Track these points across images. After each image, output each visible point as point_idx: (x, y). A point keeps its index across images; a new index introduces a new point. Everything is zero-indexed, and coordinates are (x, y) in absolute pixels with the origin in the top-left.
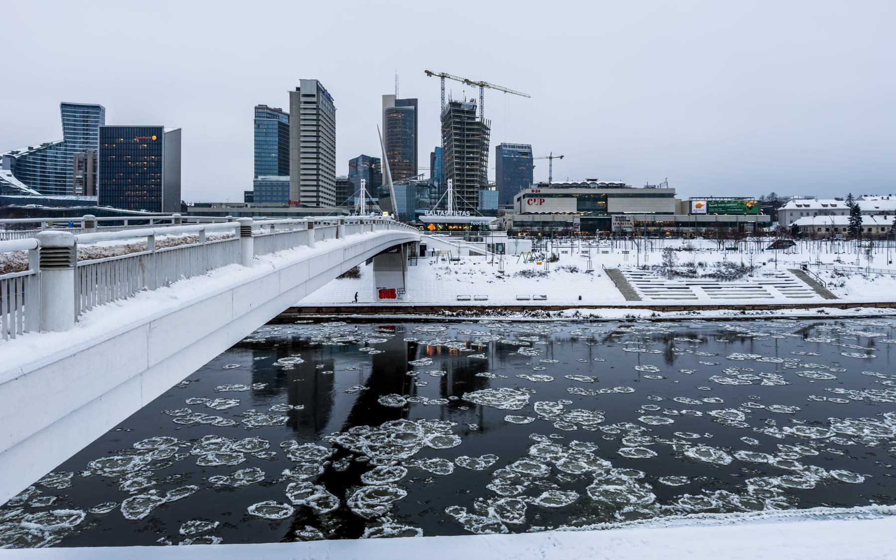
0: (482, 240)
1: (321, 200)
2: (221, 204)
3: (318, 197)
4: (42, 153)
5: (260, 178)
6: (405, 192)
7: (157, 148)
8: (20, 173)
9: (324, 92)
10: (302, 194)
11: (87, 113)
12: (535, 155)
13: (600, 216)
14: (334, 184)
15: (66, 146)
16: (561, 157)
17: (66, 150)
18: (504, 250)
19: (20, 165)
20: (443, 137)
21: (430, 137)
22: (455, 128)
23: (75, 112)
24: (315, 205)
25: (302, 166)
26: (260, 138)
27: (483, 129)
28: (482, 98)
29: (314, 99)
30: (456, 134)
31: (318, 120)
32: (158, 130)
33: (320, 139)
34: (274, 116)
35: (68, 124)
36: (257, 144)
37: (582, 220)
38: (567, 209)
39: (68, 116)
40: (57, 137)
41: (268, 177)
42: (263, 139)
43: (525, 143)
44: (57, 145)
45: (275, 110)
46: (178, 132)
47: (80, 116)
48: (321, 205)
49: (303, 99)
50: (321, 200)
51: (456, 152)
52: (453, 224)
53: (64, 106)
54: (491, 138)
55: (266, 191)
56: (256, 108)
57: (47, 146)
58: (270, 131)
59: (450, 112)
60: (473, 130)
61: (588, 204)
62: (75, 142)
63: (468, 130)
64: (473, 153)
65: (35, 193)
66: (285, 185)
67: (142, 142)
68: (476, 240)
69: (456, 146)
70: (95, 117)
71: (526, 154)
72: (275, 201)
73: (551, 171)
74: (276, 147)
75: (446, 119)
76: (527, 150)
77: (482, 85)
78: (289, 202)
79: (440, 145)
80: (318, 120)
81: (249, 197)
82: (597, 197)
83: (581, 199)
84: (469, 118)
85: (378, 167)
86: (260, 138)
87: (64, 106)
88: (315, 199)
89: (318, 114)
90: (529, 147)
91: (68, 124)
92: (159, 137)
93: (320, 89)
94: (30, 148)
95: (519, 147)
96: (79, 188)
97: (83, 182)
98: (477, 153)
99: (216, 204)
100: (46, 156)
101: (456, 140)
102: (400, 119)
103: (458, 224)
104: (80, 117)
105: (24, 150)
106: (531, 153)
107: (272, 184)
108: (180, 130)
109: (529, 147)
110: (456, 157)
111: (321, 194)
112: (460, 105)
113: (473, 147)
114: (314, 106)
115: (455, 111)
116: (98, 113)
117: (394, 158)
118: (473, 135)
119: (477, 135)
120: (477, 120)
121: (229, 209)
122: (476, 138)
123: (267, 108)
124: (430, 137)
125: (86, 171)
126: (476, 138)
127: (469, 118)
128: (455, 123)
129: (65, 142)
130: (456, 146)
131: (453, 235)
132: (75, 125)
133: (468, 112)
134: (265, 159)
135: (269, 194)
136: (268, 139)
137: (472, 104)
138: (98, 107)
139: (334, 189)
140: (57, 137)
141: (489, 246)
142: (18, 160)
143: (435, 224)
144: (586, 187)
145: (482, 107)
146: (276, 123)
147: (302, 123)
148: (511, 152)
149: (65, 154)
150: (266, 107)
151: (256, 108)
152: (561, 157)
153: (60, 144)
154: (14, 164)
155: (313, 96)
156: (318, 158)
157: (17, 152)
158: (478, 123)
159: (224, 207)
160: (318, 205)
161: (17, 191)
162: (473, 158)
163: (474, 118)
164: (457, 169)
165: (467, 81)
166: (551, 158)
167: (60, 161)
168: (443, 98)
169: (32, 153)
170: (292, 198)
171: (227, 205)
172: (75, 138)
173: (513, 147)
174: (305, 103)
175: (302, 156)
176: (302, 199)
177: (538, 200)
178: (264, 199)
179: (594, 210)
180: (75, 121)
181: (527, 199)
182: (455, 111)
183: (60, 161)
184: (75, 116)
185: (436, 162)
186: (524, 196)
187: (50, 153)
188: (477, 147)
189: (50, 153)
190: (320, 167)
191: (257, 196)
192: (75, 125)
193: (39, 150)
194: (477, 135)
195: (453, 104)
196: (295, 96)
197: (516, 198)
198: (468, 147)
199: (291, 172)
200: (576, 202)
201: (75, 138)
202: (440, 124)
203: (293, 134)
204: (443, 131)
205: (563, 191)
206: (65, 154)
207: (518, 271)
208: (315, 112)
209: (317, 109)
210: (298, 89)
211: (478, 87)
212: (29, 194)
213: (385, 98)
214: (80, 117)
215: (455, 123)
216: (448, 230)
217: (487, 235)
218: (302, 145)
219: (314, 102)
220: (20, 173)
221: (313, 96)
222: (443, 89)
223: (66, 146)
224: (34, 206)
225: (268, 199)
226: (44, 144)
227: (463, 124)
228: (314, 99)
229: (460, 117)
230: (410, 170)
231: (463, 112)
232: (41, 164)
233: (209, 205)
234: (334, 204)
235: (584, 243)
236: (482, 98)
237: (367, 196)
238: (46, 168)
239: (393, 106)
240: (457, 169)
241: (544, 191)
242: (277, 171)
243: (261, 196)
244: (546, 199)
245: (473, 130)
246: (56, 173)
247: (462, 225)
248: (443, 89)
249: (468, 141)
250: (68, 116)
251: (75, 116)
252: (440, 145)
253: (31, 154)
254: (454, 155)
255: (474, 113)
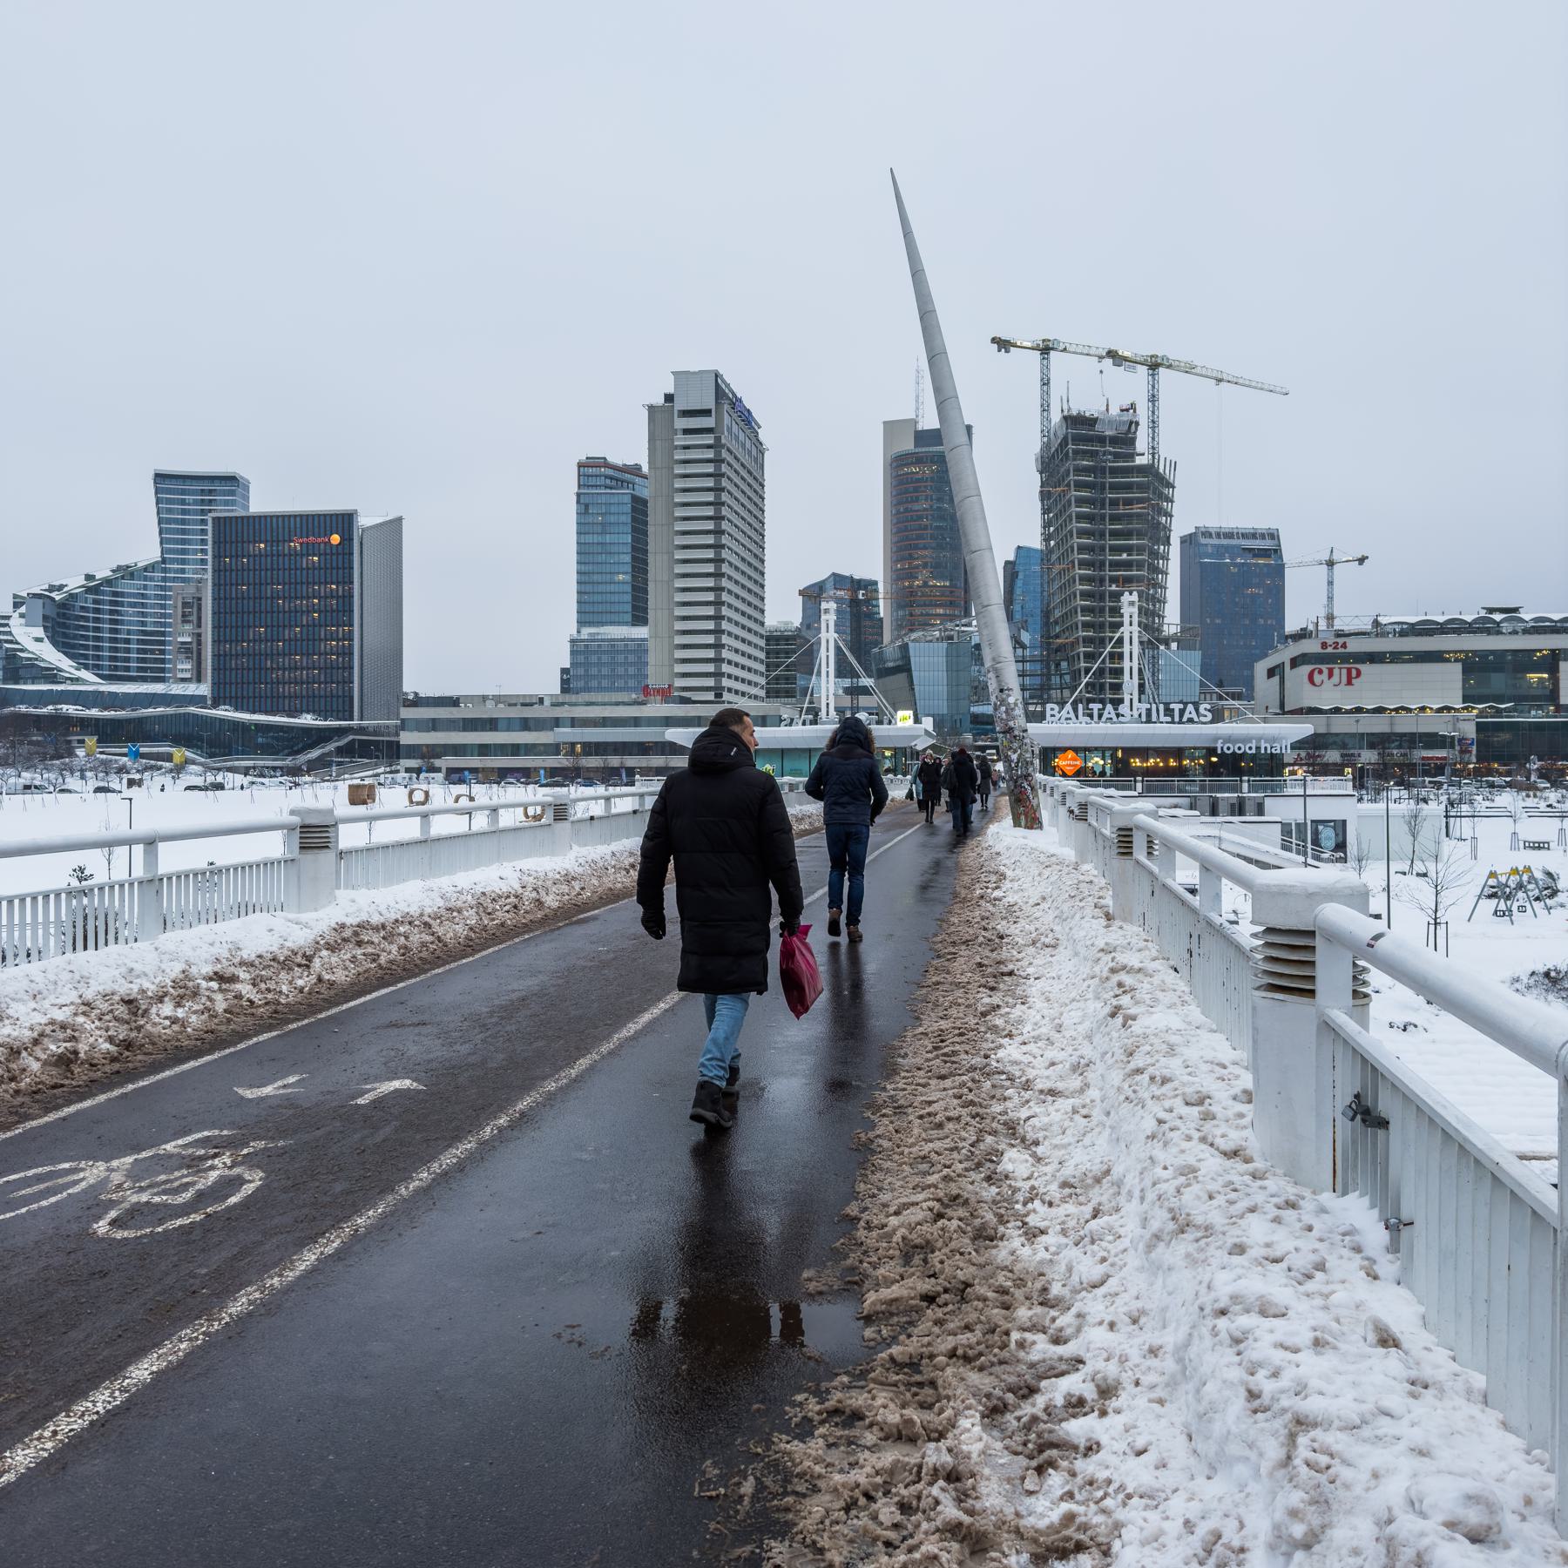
0: (1260, 810)
1: (725, 682)
2: (484, 698)
3: (718, 675)
4: (105, 593)
5: (586, 632)
6: (941, 661)
7: (340, 563)
8: (65, 635)
9: (736, 403)
10: (679, 668)
11: (210, 492)
12: (1288, 556)
13: (1535, 717)
14: (762, 643)
15: (165, 570)
16: (1362, 560)
17: (164, 579)
18: (1341, 846)
19: (63, 617)
20: (1045, 511)
21: (1007, 514)
22: (1080, 485)
23: (183, 492)
24: (710, 696)
25: (680, 597)
26: (589, 538)
27: (1155, 484)
28: (1153, 399)
29: (709, 422)
30: (1081, 502)
31: (718, 475)
32: (344, 521)
33: (725, 525)
34: (622, 483)
35: (169, 521)
36: (583, 551)
37: (1480, 727)
38: (1433, 698)
39: (169, 501)
40: (147, 550)
41: (602, 630)
42: (597, 538)
43: (1262, 524)
44: (145, 569)
45: (625, 469)
46: (394, 527)
47: (184, 494)
48: (726, 696)
49: (681, 423)
50: (725, 682)
51: (1082, 549)
52: (1143, 752)
53: (160, 477)
54: (1177, 509)
55: (626, 664)
56: (580, 465)
57: (126, 572)
58: (612, 519)
59: (1065, 439)
60: (1128, 487)
61: (1498, 682)
62: (183, 562)
63: (1114, 487)
64: (1129, 549)
65: (91, 681)
66: (640, 648)
67: (309, 550)
68: (1239, 808)
69: (1082, 533)
70: (226, 503)
71: (1265, 553)
72: (620, 690)
73: (1330, 598)
74: (628, 558)
75: (1050, 464)
76: (1266, 544)
77: (1154, 365)
78: (646, 690)
79: (1035, 542)
80: (718, 475)
81: (567, 682)
82: (1523, 661)
83: (1476, 667)
84: (1117, 456)
85: (871, 600)
86: (589, 538)
87: (160, 477)
88: (710, 682)
89: (717, 461)
90: (1273, 535)
91: (169, 521)
92: (347, 539)
93: (722, 393)
94: (89, 577)
95: (1245, 536)
96: (185, 666)
97: (192, 651)
98: (1140, 550)
99: (471, 698)
100: (122, 595)
101: (1081, 517)
102: (924, 481)
103: (1163, 752)
104: (196, 502)
105: (75, 583)
106: (1277, 551)
107: (613, 646)
108: (399, 520)
109: (1273, 535)
110: (1082, 564)
111: (725, 668)
112: (1091, 422)
113: (1127, 534)
114: (709, 439)
115: (1077, 439)
116: (232, 493)
117: (913, 577)
118: (1128, 502)
119: (1140, 501)
120: (1139, 461)
121: (502, 712)
122: (1136, 509)
123: (606, 464)
124: (1007, 514)
125: (199, 626)
126: (1136, 509)
127: (1117, 456)
128: (1078, 470)
129: (164, 561)
130: (1082, 533)
131: (1149, 791)
132: (183, 522)
133: (1114, 441)
134: (601, 588)
135: (605, 671)
136: (608, 538)
137: (1127, 417)
138: (232, 479)
139: (762, 656)
140: (147, 550)
141: (1286, 829)
142: (63, 605)
143: (1084, 751)
144: (1488, 632)
145: (1154, 424)
146: (627, 499)
147: (679, 484)
148: (1220, 551)
149: (163, 588)
150: (604, 463)
151: (580, 465)
152: (1362, 560)
153: (151, 567)
154: (52, 613)
155: (707, 413)
156: (718, 575)
157: (60, 588)
158: (1142, 470)
159: (490, 704)
160: (718, 695)
161: (51, 675)
162: (1127, 565)
163: (1132, 456)
164: (1085, 595)
165: (1112, 354)
166: (1331, 564)
167: (153, 606)
168: (1045, 408)
169: (94, 587)
170: (655, 679)
171: (498, 699)
172: (184, 552)
173: (1229, 535)
174: (686, 431)
175: (680, 569)
176: (679, 683)
177: (1340, 672)
178: (594, 684)
179: (1518, 699)
180: (184, 512)
181: (1305, 669)
182: (1077, 439)
183: (153, 606)
184: (183, 502)
185: (1019, 583)
186: (1295, 662)
187: (128, 587)
188: (1140, 535)
189: (128, 587)
190: (725, 597)
191: (578, 677)
192: (183, 522)
193: (108, 582)
194: (1140, 501)
195: (1073, 421)
196: (661, 416)
197: (1261, 668)
198: (1114, 534)
199: (651, 616)
200: (1460, 676)
201: (184, 552)
202: (1035, 480)
203: (655, 517)
204: (1044, 496)
205: (1418, 644)
206: (163, 588)
207: (1523, 973)
208: (710, 454)
209: (717, 446)
210: (669, 398)
211: (1143, 370)
212: (77, 680)
213: (891, 428)
214: (196, 502)
215: (1078, 470)
216: (1134, 773)
217: (1275, 790)
218: (679, 541)
219: (710, 435)
220: (65, 635)
221: (707, 413)
222: (1046, 383)
223: (165, 570)
224: (170, 710)
225: (605, 683)
226: (119, 568)
227: (1099, 474)
228: (709, 422)
229: (1093, 454)
230: (952, 604)
231: (1101, 440)
232: (112, 612)
233: (454, 702)
234: (762, 693)
235: (1531, 802)
236: (1153, 399)
237: (843, 670)
238: (122, 622)
239: (908, 445)
240: (1085, 595)
241: (1354, 646)
242: (628, 617)
243: (587, 676)
244: (1364, 668)
245: (1128, 487)
246: (145, 633)
247: (1179, 753)
248: (1046, 383)
249: (1115, 519)
250: (169, 501)
251: (183, 502)
252: (1035, 542)
253: (89, 590)
254: (1077, 556)
255: (1132, 442)
